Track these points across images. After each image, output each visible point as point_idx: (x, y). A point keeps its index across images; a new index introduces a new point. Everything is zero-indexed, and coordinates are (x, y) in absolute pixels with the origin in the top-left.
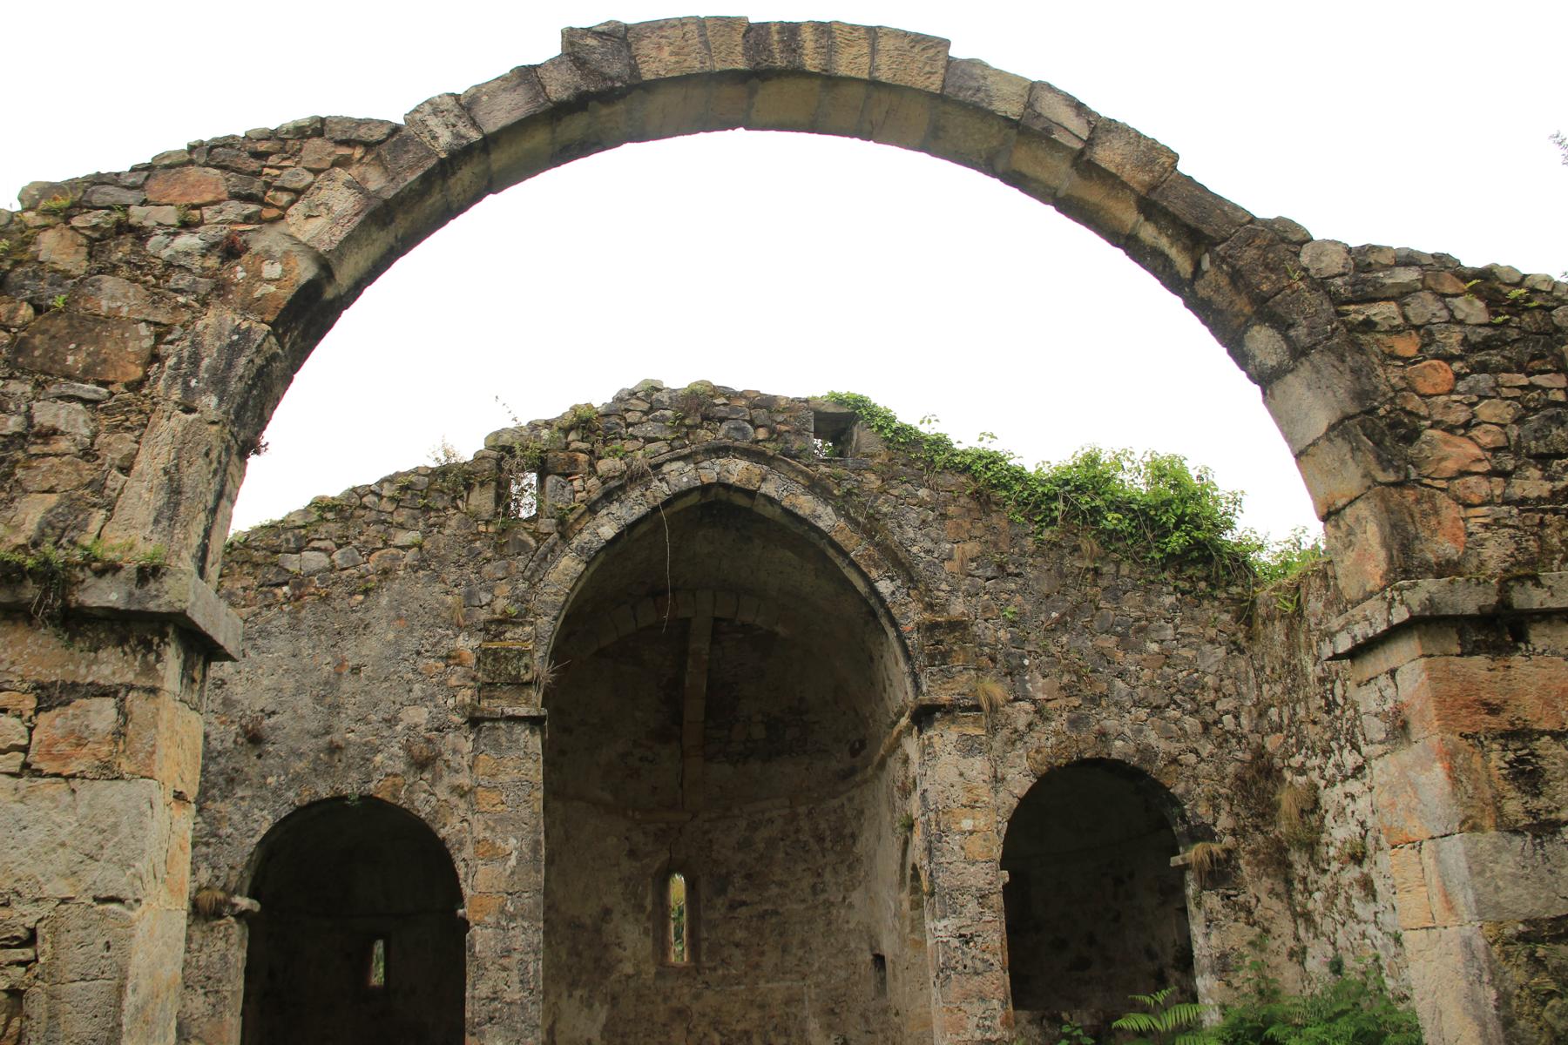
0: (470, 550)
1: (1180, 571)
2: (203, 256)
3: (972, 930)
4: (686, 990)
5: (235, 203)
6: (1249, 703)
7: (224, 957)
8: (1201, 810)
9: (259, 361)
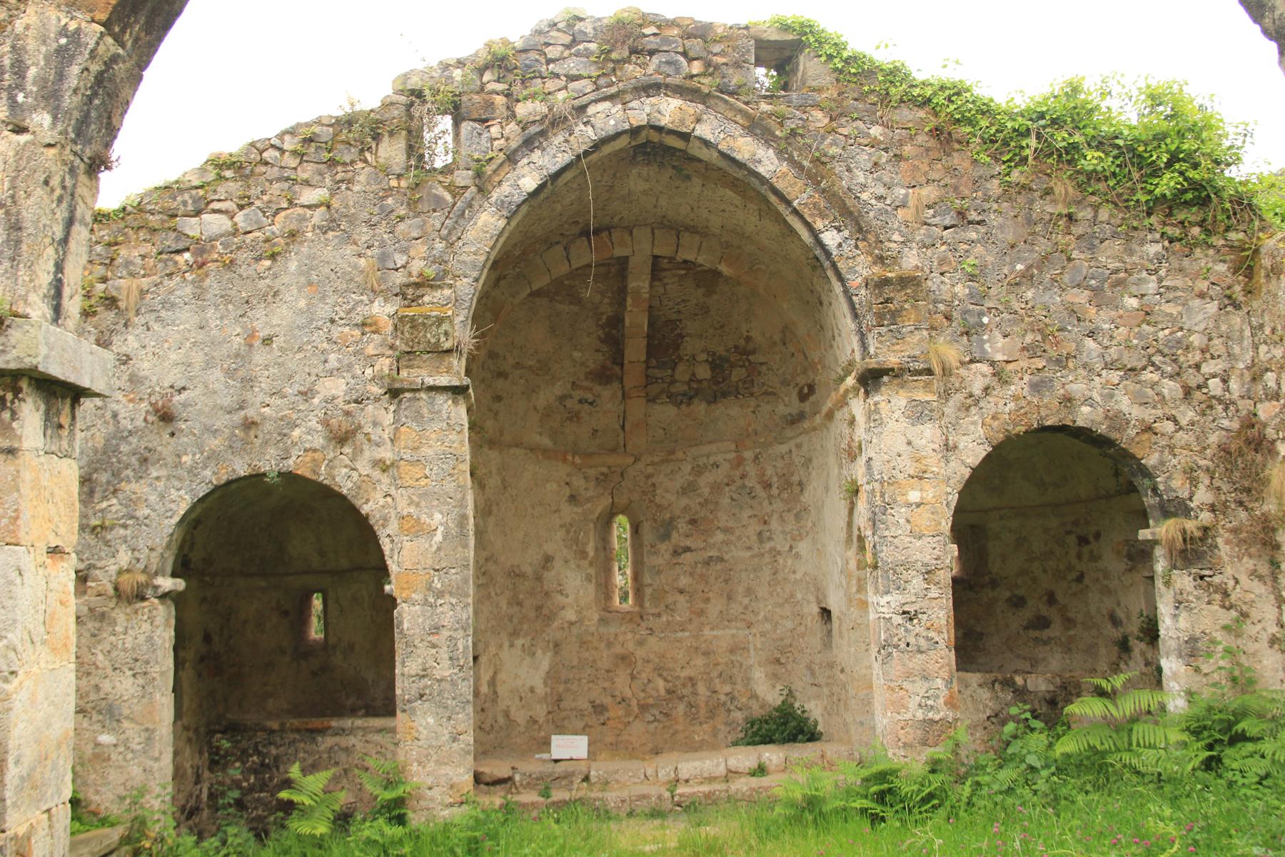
1: (1170, 215)
3: (916, 607)
4: (630, 636)
6: (1241, 366)
8: (1176, 483)
9: (95, 68)
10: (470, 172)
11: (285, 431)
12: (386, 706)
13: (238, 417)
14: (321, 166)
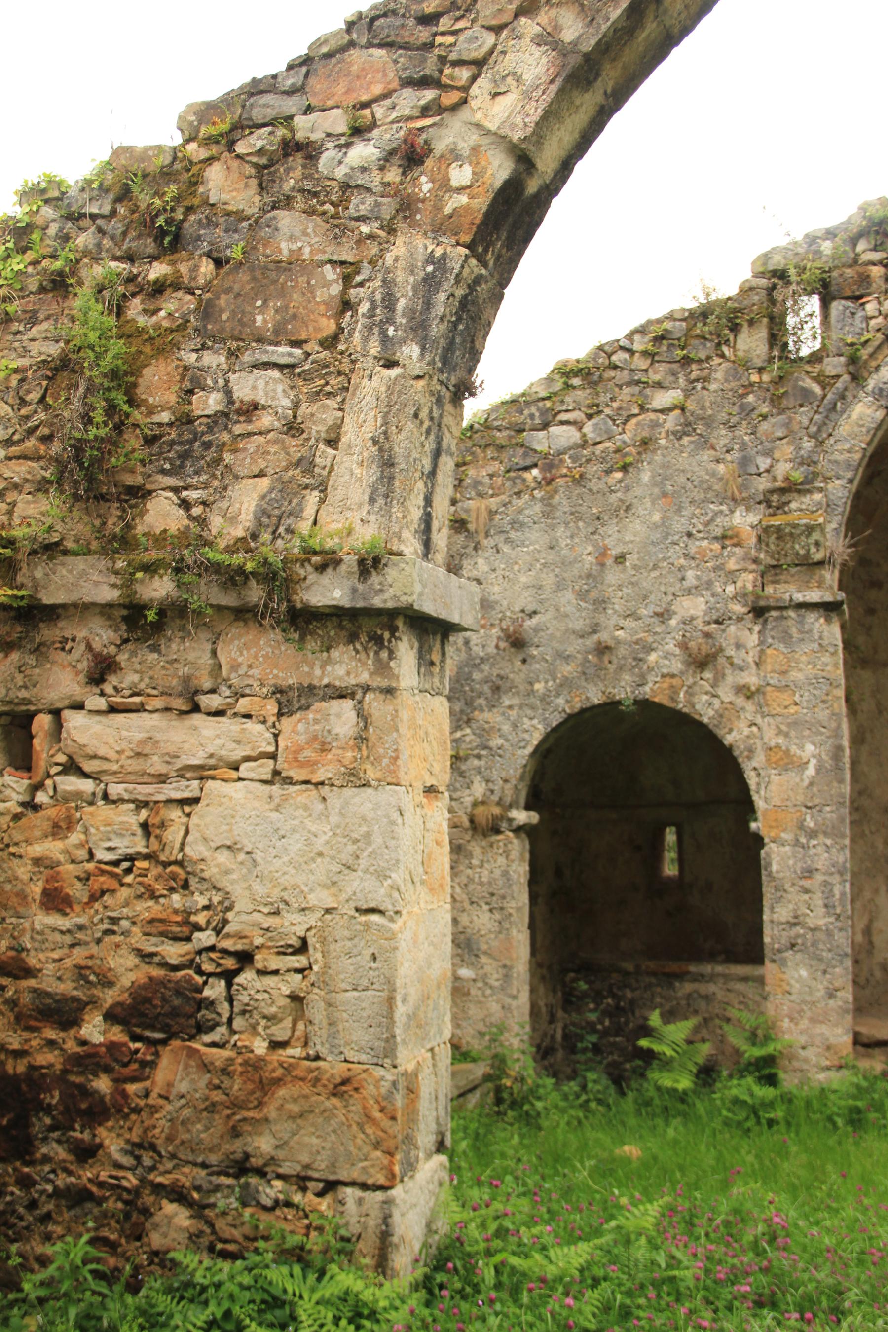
0: (742, 407)
2: (382, 169)
5: (408, 92)
7: (505, 874)
9: (460, 292)
10: (842, 359)
11: (641, 656)
12: (753, 953)
13: (591, 642)
14: (675, 366)
